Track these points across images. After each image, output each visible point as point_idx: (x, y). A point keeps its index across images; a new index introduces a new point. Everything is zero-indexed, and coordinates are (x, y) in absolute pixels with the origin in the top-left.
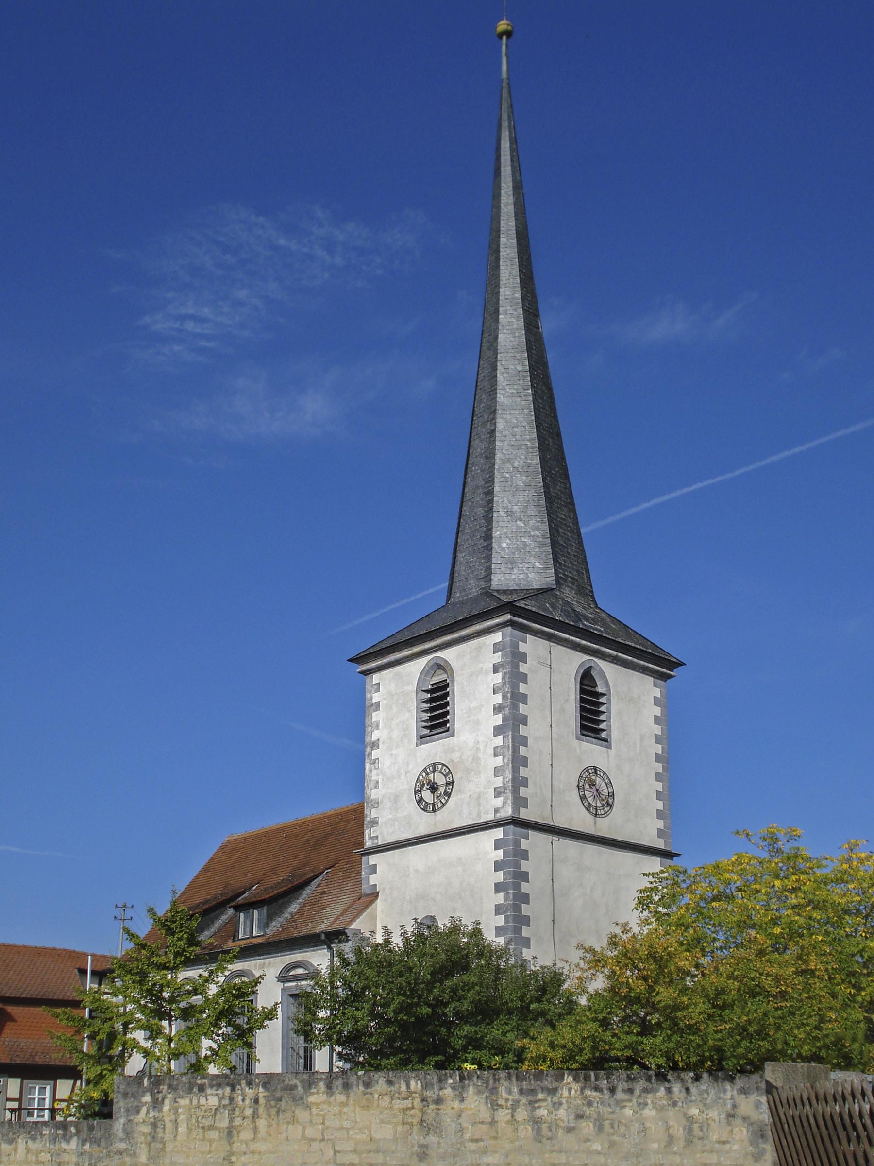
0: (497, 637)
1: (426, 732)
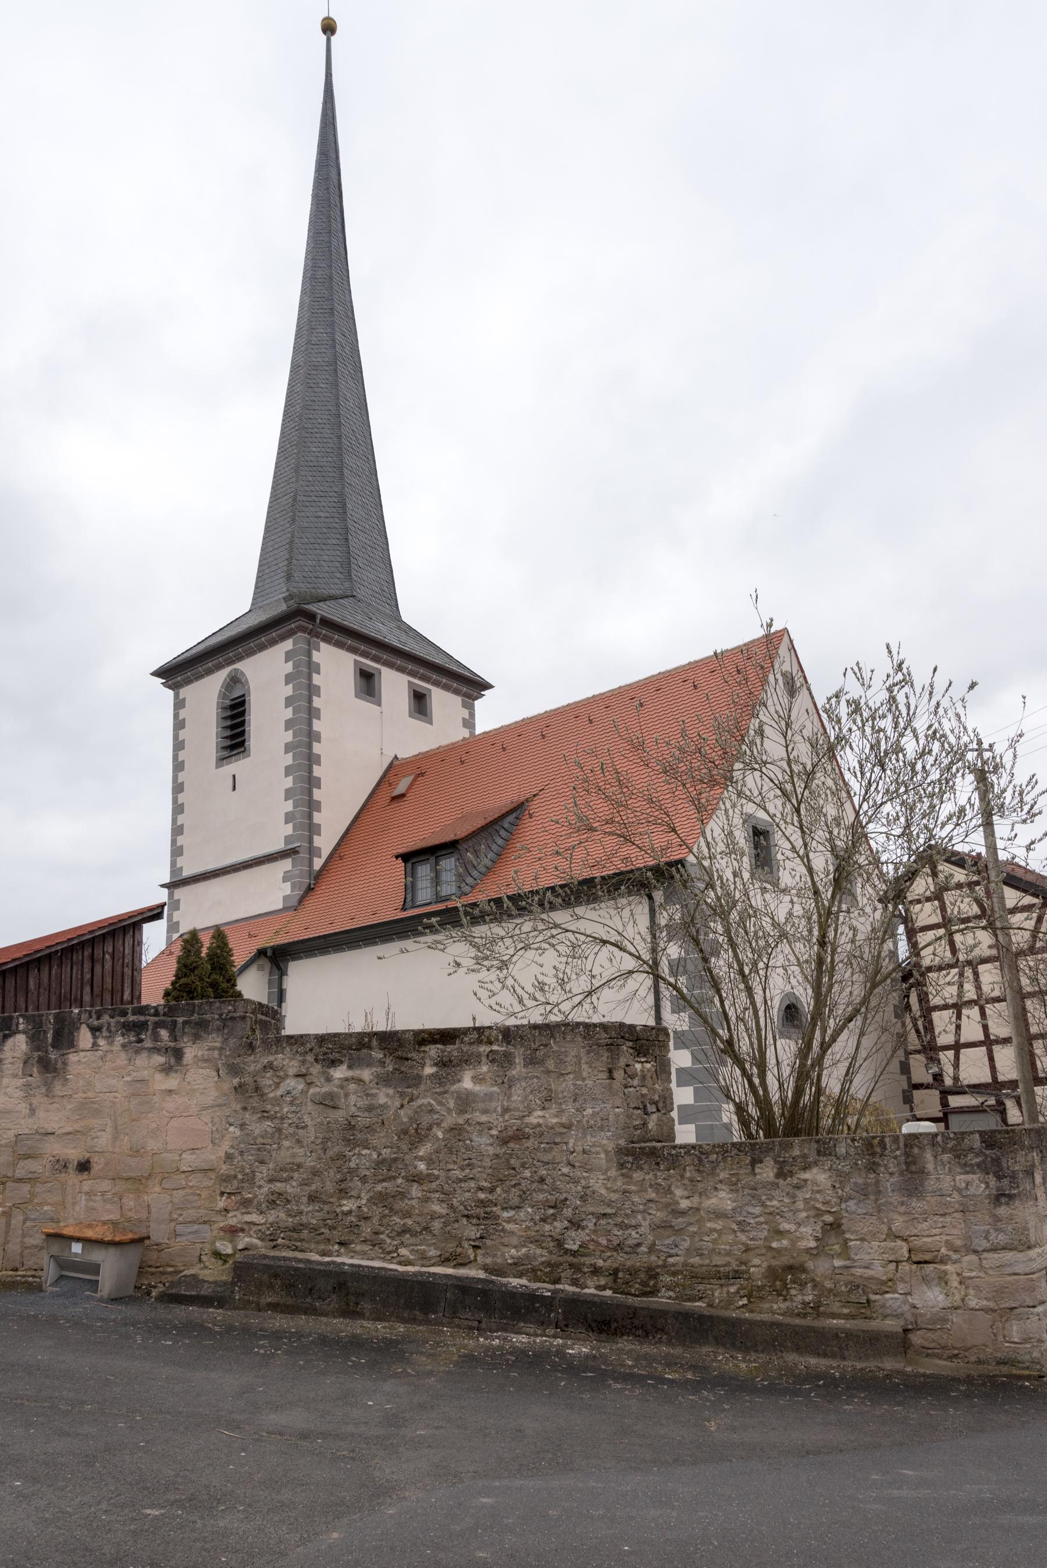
0: (288, 645)
1: (226, 753)
